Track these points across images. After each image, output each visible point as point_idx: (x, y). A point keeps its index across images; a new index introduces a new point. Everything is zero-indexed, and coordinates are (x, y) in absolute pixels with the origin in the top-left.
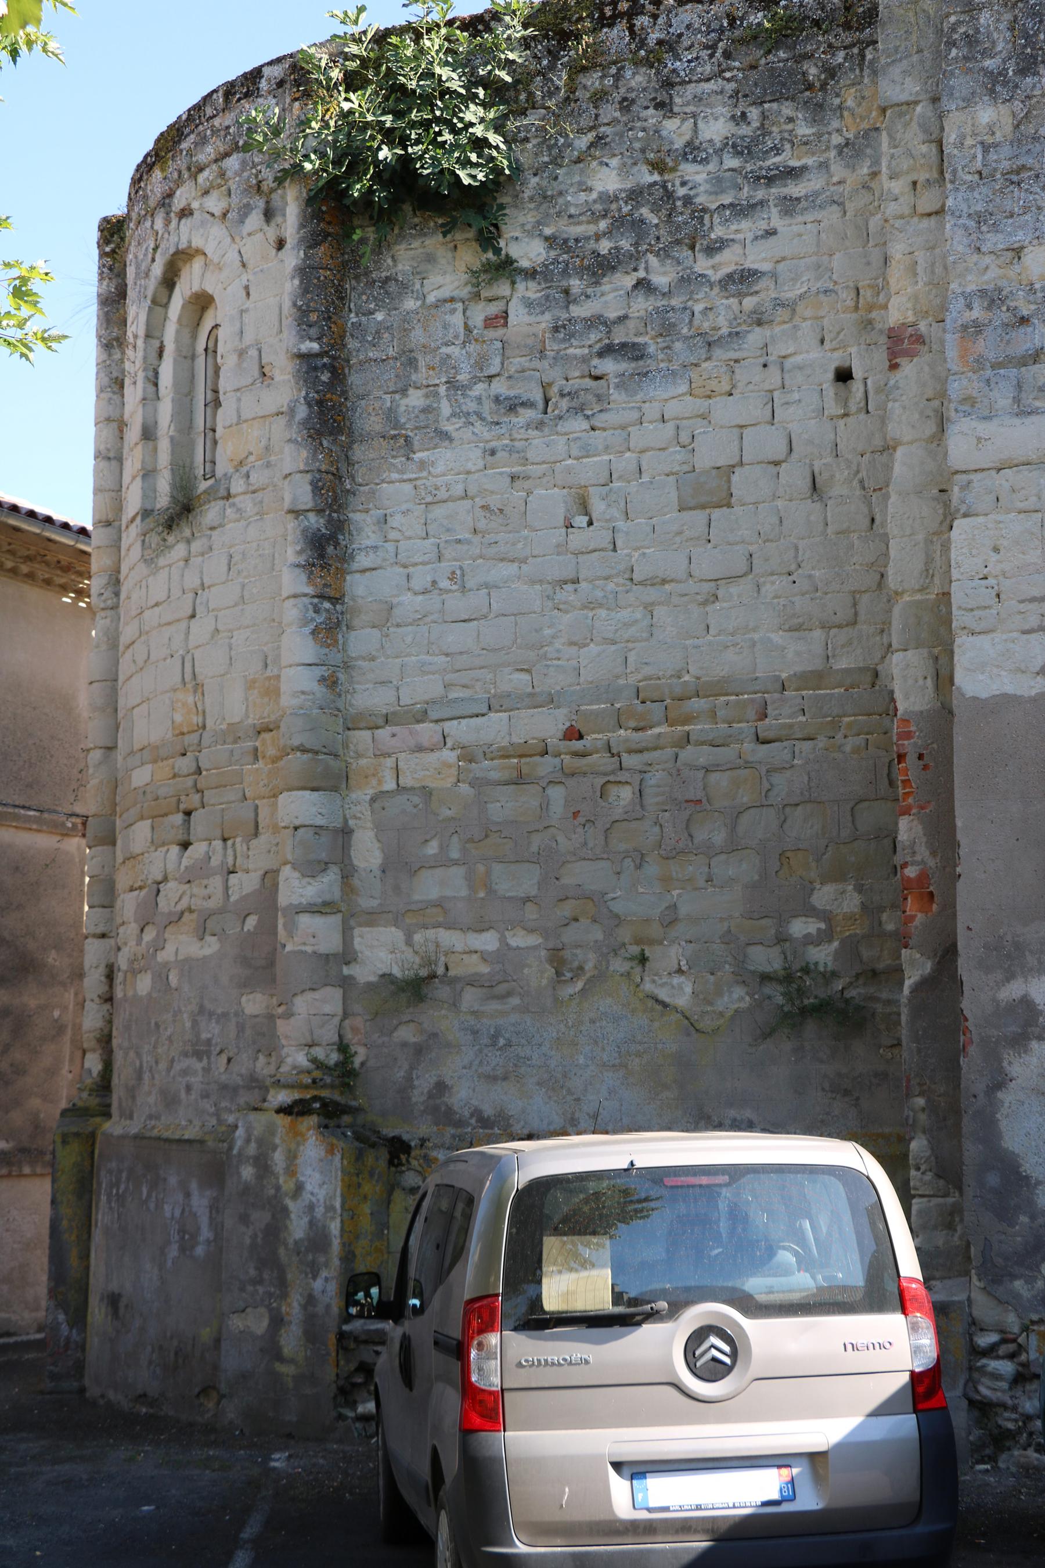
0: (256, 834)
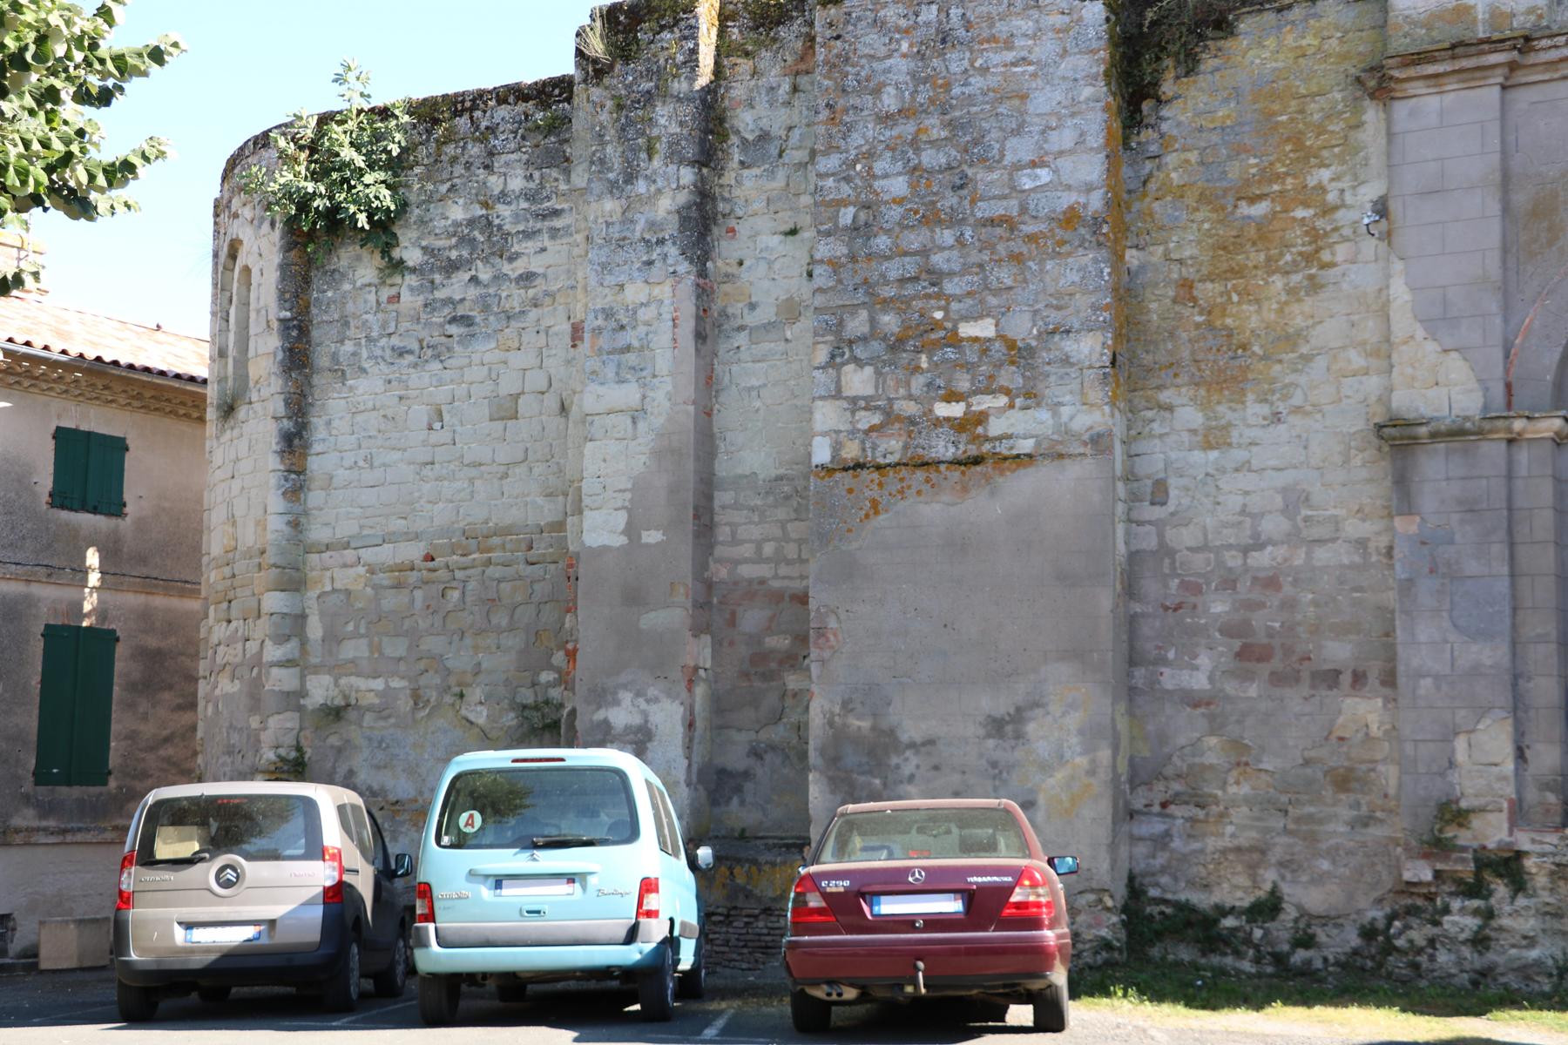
0: (259, 617)
